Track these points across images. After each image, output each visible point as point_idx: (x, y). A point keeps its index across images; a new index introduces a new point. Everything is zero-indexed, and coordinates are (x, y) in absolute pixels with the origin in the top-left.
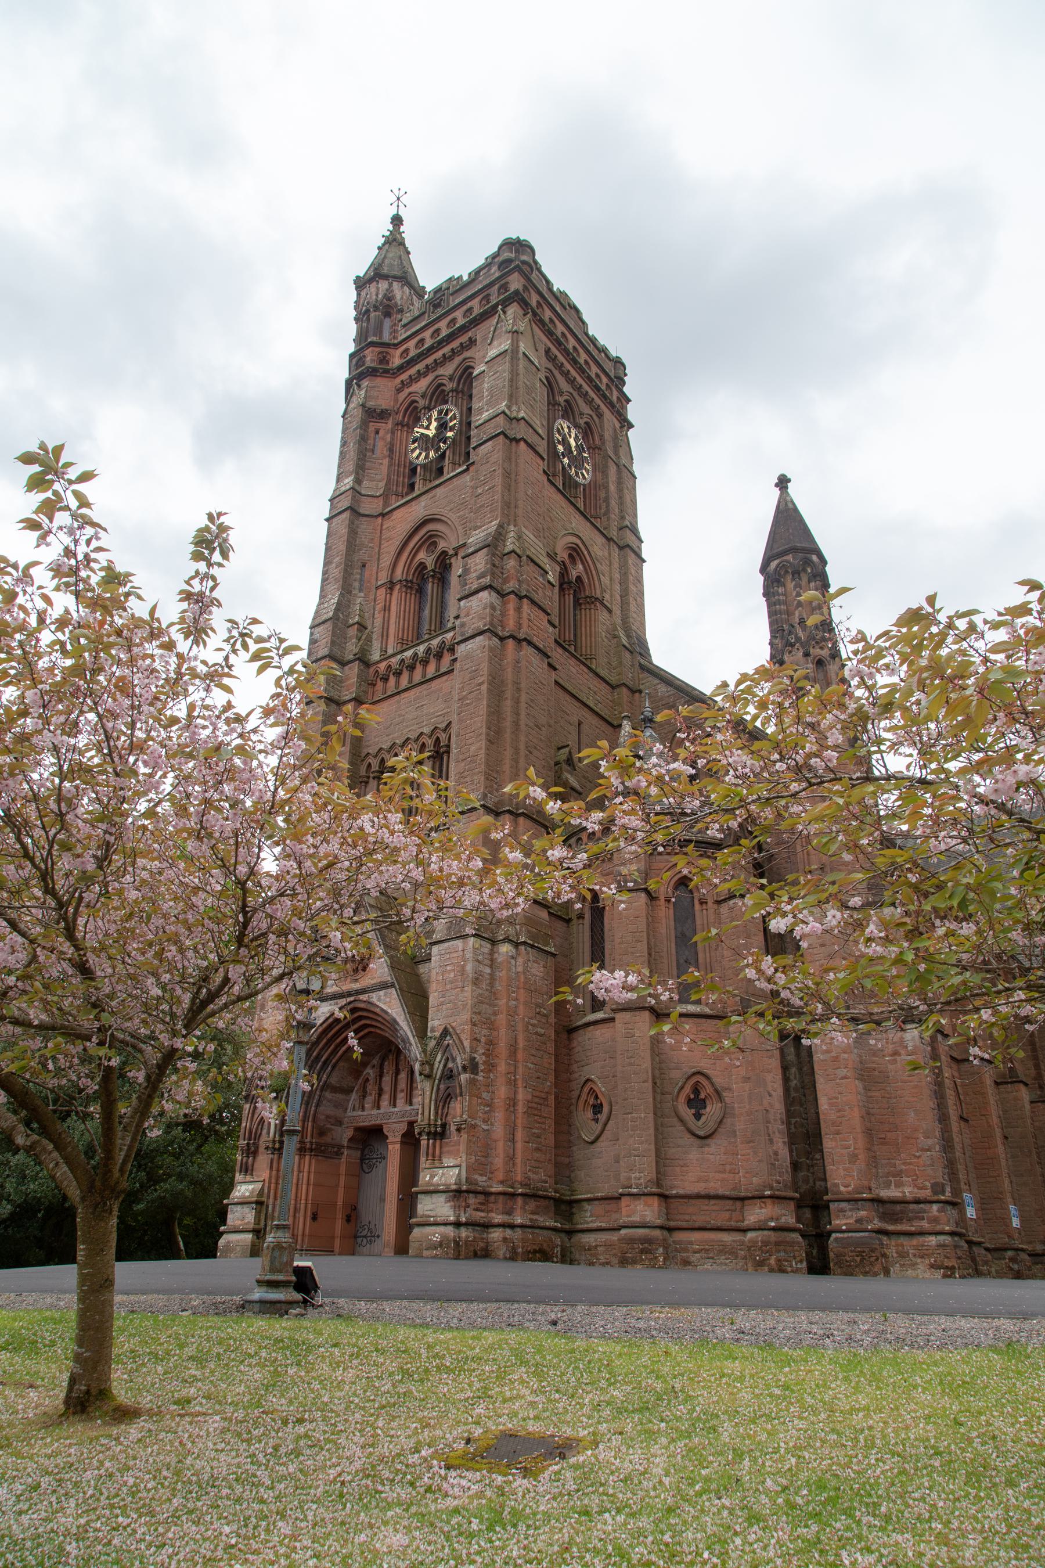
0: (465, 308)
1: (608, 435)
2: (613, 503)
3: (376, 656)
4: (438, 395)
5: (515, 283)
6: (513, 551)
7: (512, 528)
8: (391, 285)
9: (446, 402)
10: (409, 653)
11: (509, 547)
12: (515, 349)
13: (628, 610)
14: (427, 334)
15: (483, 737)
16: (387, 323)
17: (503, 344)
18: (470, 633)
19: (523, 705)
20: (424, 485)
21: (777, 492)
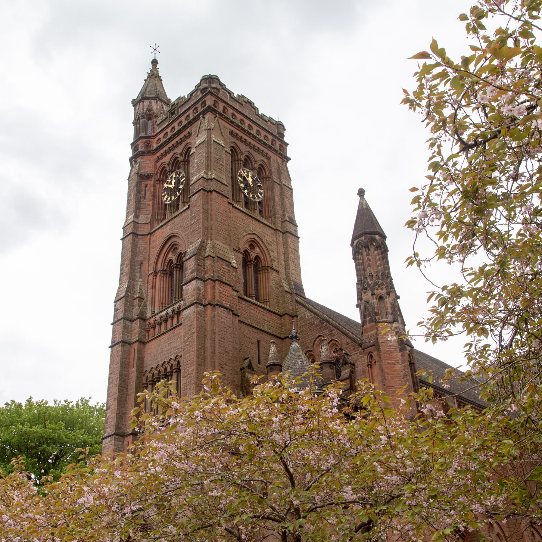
0: (186, 115)
1: (273, 169)
2: (278, 208)
3: (149, 315)
4: (175, 164)
5: (210, 101)
6: (209, 256)
7: (209, 241)
8: (150, 102)
9: (179, 168)
10: (164, 313)
11: (208, 253)
12: (209, 139)
13: (289, 269)
14: (168, 130)
15: (195, 363)
16: (150, 123)
17: (202, 137)
18: (188, 304)
19: (217, 342)
20: (171, 215)
21: (358, 198)
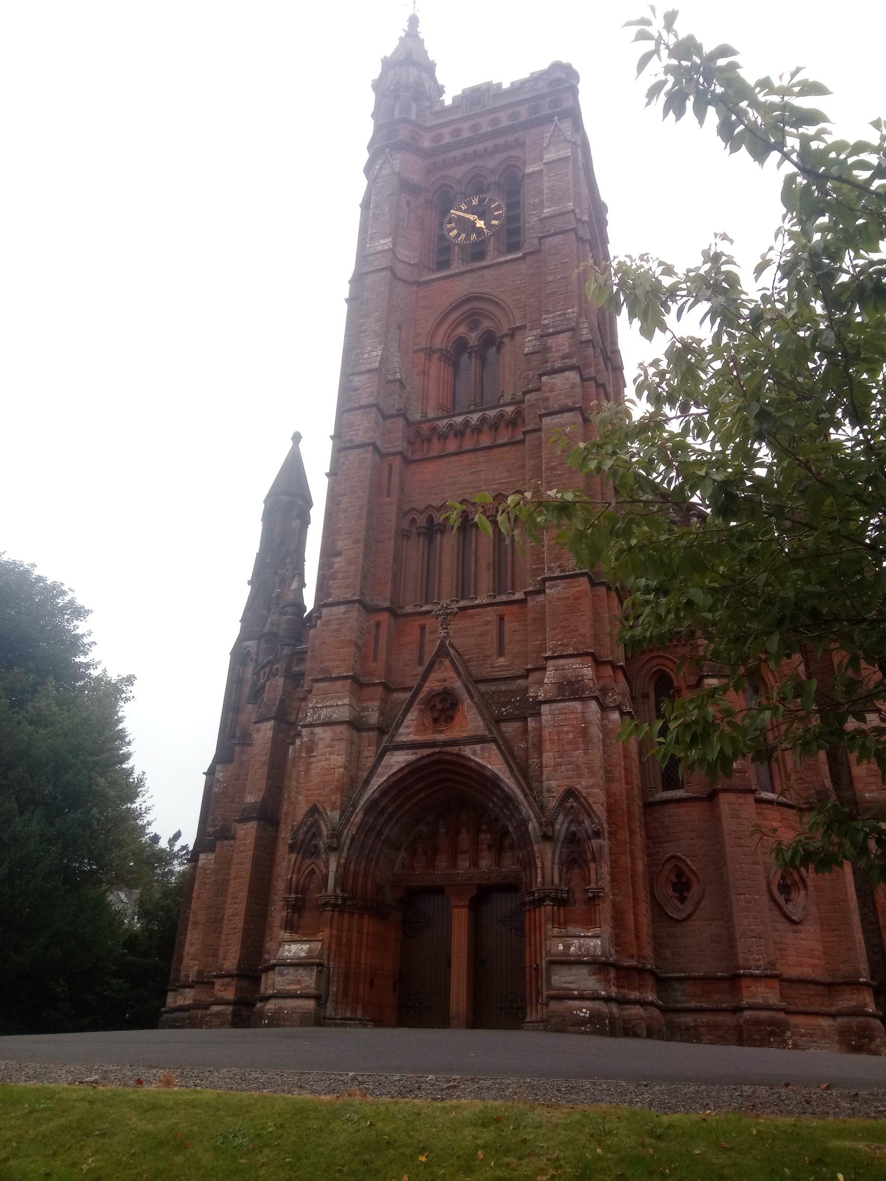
0: (492, 116)
10: (459, 419)
18: (556, 407)
21: (291, 444)
